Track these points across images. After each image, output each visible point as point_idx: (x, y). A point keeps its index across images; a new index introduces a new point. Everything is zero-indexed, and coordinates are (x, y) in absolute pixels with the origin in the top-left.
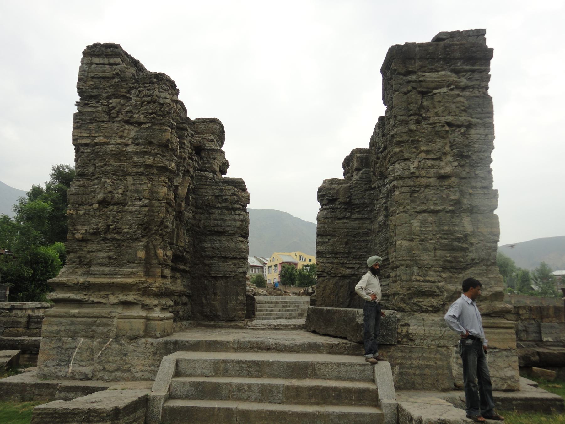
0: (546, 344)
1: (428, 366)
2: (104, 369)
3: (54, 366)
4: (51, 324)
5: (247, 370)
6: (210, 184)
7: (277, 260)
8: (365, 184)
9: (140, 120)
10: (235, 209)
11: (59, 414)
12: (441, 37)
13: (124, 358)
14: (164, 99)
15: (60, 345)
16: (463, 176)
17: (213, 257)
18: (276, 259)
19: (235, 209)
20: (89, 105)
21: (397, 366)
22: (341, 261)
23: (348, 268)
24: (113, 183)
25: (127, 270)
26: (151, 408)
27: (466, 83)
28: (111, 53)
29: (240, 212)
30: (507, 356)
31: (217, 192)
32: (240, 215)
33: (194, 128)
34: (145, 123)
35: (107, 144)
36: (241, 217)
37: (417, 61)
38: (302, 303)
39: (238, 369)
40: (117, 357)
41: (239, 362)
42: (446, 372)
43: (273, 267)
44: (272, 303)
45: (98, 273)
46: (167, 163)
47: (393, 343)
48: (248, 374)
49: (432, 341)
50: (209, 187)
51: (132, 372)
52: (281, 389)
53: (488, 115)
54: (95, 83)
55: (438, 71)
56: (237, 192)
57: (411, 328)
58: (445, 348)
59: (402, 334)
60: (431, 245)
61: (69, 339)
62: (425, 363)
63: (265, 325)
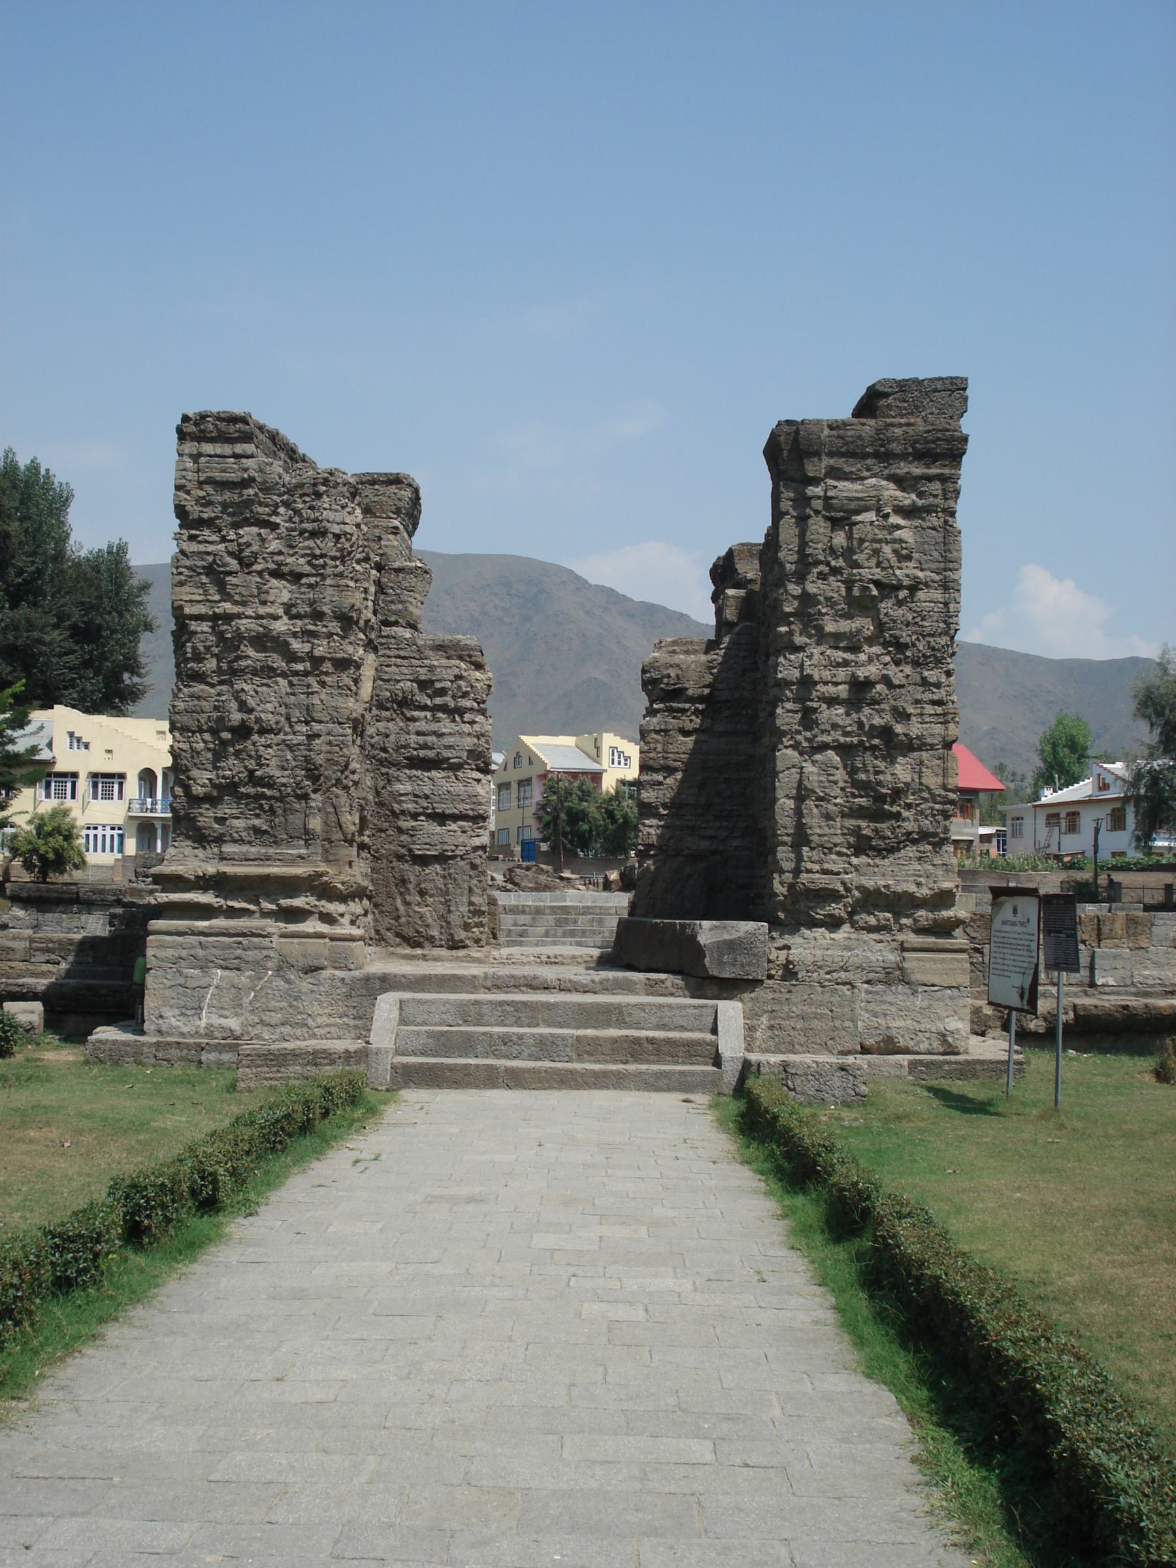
0: (1104, 990)
1: (816, 1016)
2: (262, 1022)
3: (174, 1017)
4: (163, 946)
5: (514, 1016)
6: (407, 654)
7: (531, 763)
8: (745, 657)
9: (299, 570)
10: (461, 711)
11: (275, 1055)
12: (880, 388)
13: (295, 1003)
14: (342, 526)
15: (182, 981)
16: (897, 682)
17: (419, 814)
18: (525, 761)
19: (461, 711)
20: (199, 539)
21: (765, 1016)
22: (690, 824)
23: (704, 838)
24: (257, 692)
25: (289, 852)
26: (374, 1065)
27: (914, 502)
28: (236, 435)
29: (472, 717)
30: (952, 998)
31: (423, 674)
32: (472, 723)
33: (380, 548)
34: (308, 575)
35: (239, 616)
36: (476, 727)
37: (824, 457)
38: (613, 911)
39: (500, 1014)
40: (282, 1001)
41: (501, 1003)
42: (847, 1024)
43: (514, 786)
44: (523, 912)
45: (236, 857)
46: (350, 649)
47: (760, 978)
48: (516, 1022)
49: (828, 973)
50: (405, 662)
51: (309, 1028)
52: (570, 1041)
53: (951, 565)
54: (208, 495)
55: (863, 479)
56: (465, 670)
57: (791, 952)
58: (849, 987)
59: (778, 963)
60: (835, 808)
61: (196, 972)
62: (814, 1010)
63: (528, 956)
